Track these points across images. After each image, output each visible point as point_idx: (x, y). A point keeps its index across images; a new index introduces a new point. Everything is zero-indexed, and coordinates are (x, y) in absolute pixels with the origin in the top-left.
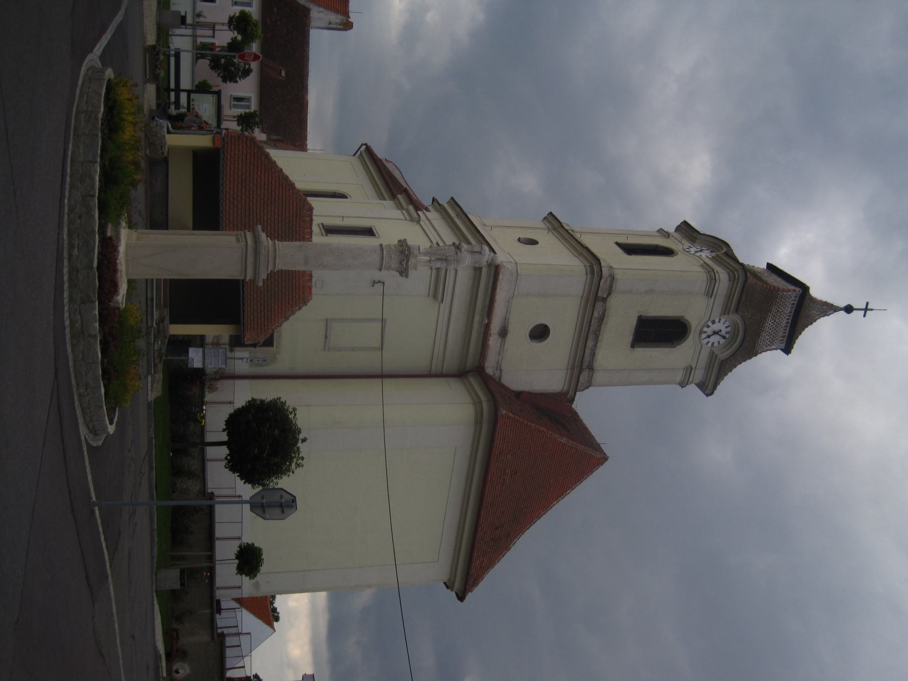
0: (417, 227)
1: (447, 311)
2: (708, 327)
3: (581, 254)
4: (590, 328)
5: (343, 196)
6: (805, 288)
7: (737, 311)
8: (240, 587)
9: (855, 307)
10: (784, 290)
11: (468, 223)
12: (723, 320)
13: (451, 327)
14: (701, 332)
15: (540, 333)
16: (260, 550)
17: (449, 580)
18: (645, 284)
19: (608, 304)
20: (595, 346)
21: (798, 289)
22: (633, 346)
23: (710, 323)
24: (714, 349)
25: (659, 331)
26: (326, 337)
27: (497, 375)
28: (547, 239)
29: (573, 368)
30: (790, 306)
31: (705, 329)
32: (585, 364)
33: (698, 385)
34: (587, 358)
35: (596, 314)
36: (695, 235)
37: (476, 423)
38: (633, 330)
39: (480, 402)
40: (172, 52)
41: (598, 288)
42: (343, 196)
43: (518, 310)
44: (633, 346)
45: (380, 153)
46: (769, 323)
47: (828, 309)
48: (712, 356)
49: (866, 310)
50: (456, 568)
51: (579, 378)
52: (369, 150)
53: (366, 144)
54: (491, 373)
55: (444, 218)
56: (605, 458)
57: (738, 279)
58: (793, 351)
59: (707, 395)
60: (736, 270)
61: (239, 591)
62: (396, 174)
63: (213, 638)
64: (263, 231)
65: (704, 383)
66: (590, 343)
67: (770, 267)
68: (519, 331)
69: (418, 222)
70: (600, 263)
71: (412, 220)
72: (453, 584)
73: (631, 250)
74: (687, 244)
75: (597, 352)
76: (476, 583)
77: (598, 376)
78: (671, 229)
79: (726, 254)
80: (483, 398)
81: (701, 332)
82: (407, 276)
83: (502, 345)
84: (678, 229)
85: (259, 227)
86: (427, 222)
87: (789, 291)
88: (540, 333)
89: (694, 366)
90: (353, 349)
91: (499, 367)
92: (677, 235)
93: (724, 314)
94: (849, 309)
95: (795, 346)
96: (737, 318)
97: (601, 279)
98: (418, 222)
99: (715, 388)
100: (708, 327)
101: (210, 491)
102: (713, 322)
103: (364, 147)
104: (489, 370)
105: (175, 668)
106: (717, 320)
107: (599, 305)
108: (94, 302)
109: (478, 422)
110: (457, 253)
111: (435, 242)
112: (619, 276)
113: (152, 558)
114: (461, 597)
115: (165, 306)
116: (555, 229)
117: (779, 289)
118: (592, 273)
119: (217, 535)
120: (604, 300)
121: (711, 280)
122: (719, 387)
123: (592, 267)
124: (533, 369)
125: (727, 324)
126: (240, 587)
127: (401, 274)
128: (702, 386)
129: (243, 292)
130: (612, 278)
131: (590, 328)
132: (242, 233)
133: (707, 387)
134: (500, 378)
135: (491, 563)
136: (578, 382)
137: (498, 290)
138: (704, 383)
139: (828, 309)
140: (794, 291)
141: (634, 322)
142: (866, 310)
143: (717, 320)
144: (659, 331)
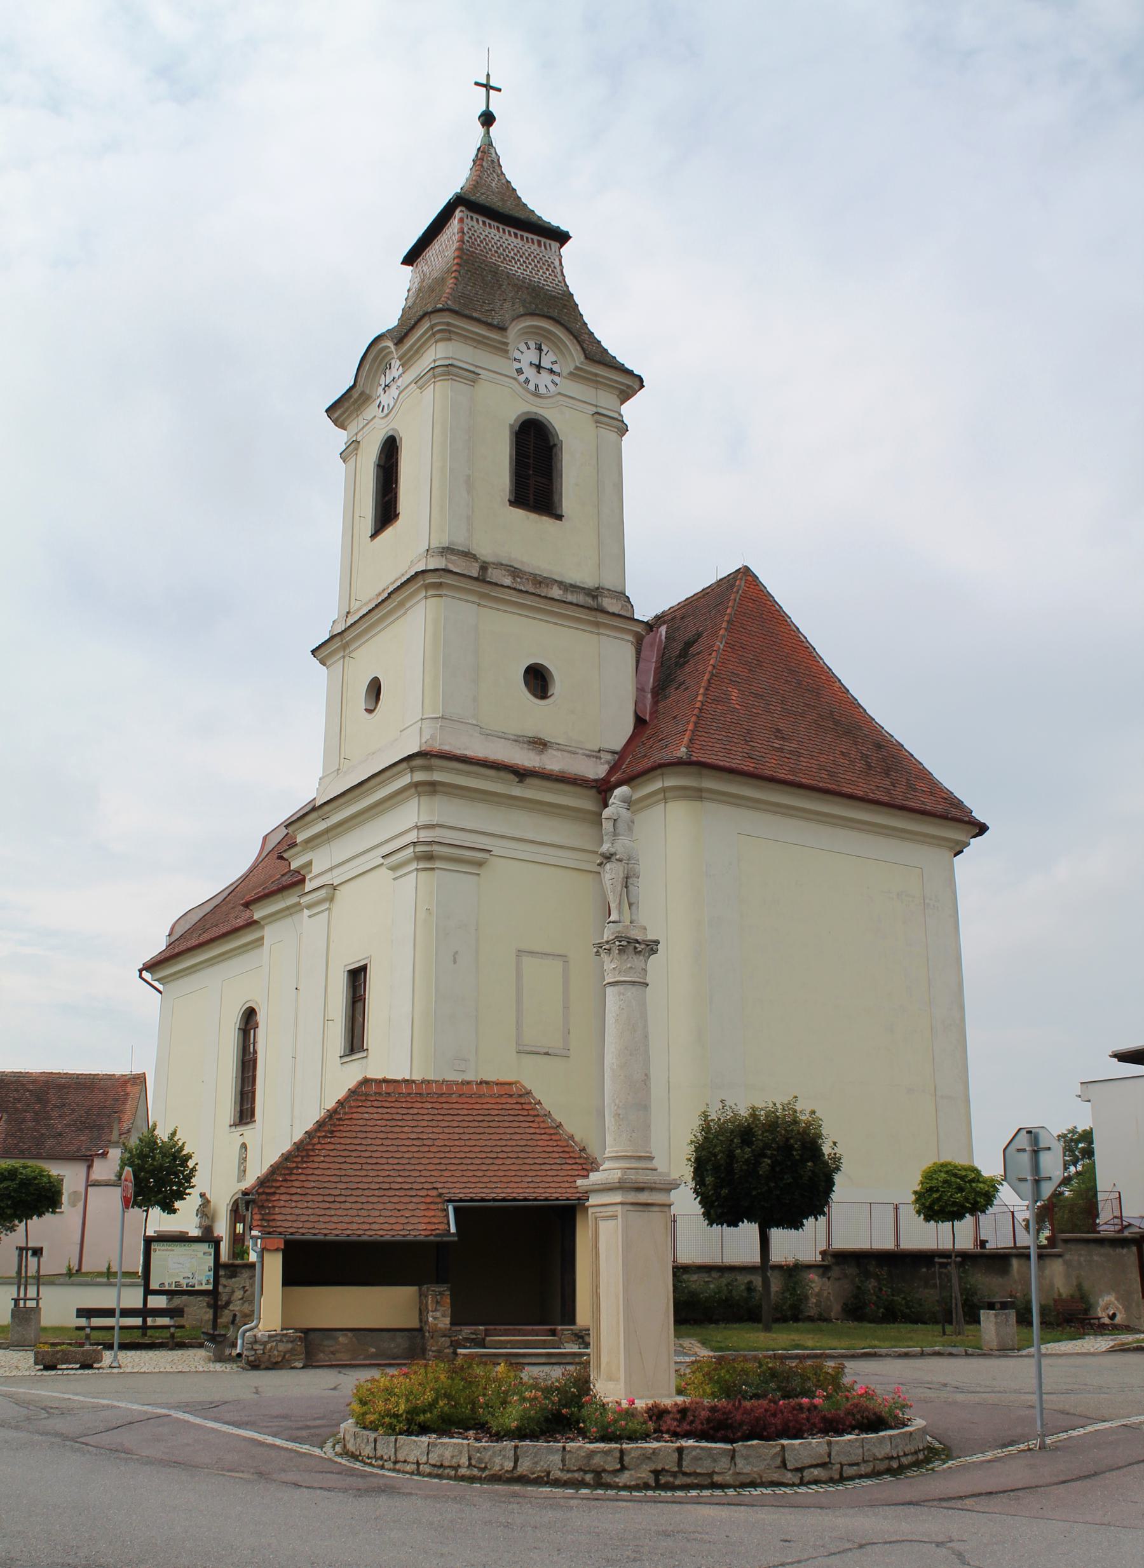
0: (344, 889)
1: (504, 843)
2: (527, 381)
3: (401, 604)
4: (532, 591)
5: (250, 1015)
6: (458, 202)
7: (502, 329)
8: (897, 1208)
9: (484, 108)
10: (462, 241)
11: (342, 800)
12: (517, 355)
13: (530, 836)
14: (536, 394)
15: (538, 680)
16: (929, 1176)
17: (951, 848)
18: (454, 487)
19: (489, 559)
20: (561, 584)
21: (458, 214)
22: (559, 517)
23: (522, 378)
24: (565, 372)
25: (534, 469)
26: (547, 1054)
27: (609, 757)
28: (368, 660)
29: (597, 624)
30: (488, 230)
31: (532, 387)
32: (590, 602)
33: (623, 403)
34: (581, 599)
35: (507, 581)
36: (355, 394)
37: (700, 798)
38: (533, 516)
39: (664, 790)
40: (83, 1322)
41: (461, 574)
42: (250, 1015)
43: (504, 721)
44: (559, 517)
45: (157, 945)
46: (517, 269)
47: (486, 159)
48: (577, 375)
49: (488, 87)
50: (933, 837)
51: (614, 614)
52: (151, 966)
53: (141, 971)
54: (607, 767)
55: (329, 840)
56: (745, 573)
57: (448, 324)
58: (564, 228)
59: (642, 386)
60: (432, 327)
61: (902, 1208)
62: (195, 918)
63: (1060, 1256)
64: (587, 1176)
65: (622, 391)
66: (556, 592)
67: (410, 259)
68: (536, 716)
69: (334, 888)
70: (423, 572)
71: (331, 899)
72: (957, 842)
73: (386, 512)
74: (371, 411)
75: (568, 581)
76: (958, 804)
77: (609, 582)
78: (340, 438)
79: (399, 342)
80: (657, 785)
81: (536, 394)
82: (657, 942)
83: (559, 747)
84: (340, 424)
85: (579, 1182)
86: (336, 872)
87: (461, 231)
88: (538, 680)
89: (595, 410)
90: (566, 1007)
91: (596, 755)
92: (354, 426)
93: (507, 351)
94: (487, 119)
95: (555, 223)
96: (514, 329)
97: (451, 572)
98: (334, 888)
99: (630, 373)
100: (527, 381)
101: (819, 1258)
102: (520, 371)
103: (145, 974)
104: (597, 770)
105: (1106, 1321)
106: (517, 365)
107: (494, 575)
108: (783, 1446)
109: (698, 795)
110: (620, 860)
111: (382, 861)
112: (441, 539)
113: (922, 1355)
114: (982, 829)
115: (553, 1333)
116: (345, 646)
117: (460, 249)
118: (440, 585)
119: (888, 1244)
120: (484, 567)
121: (449, 374)
122: (628, 365)
123: (427, 587)
124: (599, 695)
125: (523, 347)
126: (897, 1208)
127: (654, 952)
128: (626, 395)
129: (525, 1200)
130: (446, 551)
131: (532, 591)
132: (590, 1211)
133: (629, 387)
134: (614, 753)
135: (925, 775)
136: (619, 616)
137: (469, 753)
138: (622, 391)
139: (486, 159)
140: (461, 220)
141: (519, 513)
142: (488, 87)
143: (517, 365)
144: (534, 469)
